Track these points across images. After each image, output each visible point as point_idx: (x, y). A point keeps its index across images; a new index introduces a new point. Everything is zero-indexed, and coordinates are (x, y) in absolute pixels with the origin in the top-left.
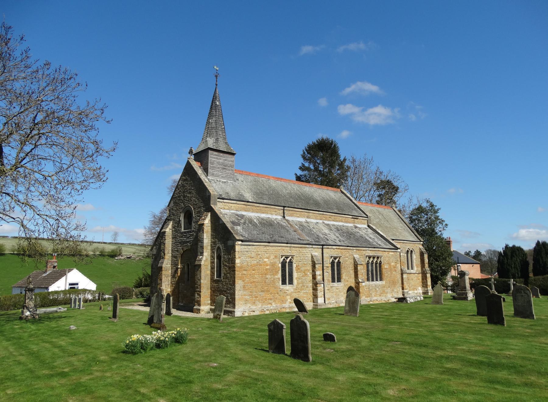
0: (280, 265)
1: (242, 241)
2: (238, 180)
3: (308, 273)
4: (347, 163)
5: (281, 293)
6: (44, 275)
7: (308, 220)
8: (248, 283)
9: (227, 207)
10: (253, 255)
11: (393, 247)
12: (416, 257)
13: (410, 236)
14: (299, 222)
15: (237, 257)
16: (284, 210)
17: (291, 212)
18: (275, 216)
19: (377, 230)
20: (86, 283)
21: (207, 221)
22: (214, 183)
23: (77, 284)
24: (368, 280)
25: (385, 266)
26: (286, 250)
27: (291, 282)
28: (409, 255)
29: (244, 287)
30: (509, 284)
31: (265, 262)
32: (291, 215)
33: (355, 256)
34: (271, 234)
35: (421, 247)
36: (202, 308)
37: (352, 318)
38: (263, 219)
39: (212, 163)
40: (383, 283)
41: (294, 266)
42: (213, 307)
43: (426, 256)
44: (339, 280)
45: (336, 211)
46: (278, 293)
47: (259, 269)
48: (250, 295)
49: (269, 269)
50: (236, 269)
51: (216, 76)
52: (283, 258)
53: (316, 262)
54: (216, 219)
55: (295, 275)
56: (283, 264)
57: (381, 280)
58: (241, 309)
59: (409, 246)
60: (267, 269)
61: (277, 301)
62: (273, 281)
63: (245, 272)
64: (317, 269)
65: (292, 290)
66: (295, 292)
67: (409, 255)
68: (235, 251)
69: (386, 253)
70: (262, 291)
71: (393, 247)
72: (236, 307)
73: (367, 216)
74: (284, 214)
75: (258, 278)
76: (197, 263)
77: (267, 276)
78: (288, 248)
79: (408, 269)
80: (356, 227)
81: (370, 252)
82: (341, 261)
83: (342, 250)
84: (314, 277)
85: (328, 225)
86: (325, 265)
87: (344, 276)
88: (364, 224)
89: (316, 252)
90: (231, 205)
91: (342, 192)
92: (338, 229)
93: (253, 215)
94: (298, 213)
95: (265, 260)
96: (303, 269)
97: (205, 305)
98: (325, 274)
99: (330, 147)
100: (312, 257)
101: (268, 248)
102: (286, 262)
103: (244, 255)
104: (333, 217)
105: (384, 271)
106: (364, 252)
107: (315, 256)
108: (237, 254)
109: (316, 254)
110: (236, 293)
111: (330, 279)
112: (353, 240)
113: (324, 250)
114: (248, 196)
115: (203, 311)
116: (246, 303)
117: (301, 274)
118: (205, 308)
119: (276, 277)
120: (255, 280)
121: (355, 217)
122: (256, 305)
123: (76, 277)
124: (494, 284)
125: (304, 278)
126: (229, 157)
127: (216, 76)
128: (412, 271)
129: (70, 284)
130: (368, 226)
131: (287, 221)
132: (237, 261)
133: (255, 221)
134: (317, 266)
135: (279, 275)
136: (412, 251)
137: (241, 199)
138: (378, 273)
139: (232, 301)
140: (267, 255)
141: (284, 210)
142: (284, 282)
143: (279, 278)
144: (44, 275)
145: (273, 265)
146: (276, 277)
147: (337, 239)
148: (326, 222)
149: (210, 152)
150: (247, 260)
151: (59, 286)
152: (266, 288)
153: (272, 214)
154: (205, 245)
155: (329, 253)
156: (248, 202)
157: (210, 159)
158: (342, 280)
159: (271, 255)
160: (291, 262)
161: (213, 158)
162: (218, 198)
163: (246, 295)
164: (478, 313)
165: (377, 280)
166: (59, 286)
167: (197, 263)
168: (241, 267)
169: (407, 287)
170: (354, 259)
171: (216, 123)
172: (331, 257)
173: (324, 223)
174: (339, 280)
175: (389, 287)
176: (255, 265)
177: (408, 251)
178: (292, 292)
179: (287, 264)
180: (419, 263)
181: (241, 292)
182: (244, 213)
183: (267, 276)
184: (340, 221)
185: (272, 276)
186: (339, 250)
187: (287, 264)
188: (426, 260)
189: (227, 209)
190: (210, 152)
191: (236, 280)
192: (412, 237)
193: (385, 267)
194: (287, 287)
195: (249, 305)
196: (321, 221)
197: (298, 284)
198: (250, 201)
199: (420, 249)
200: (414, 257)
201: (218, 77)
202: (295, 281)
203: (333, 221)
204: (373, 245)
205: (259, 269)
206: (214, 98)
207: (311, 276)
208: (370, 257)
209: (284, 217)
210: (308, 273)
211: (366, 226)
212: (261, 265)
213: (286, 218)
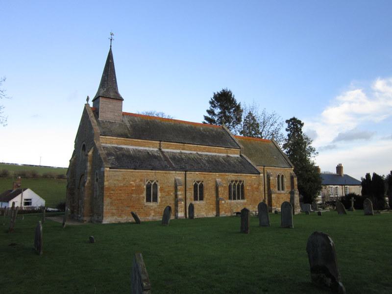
0: (145, 187)
3: (172, 193)
8: (115, 200)
9: (109, 142)
10: (120, 178)
12: (287, 181)
15: (105, 180)
16: (160, 143)
23: (31, 200)
24: (230, 198)
25: (247, 188)
27: (155, 200)
30: (351, 202)
31: (131, 184)
32: (168, 148)
33: (217, 180)
35: (292, 172)
40: (245, 201)
43: (295, 179)
48: (116, 210)
51: (111, 40)
53: (178, 184)
55: (159, 194)
56: (149, 187)
58: (106, 220)
63: (112, 192)
69: (249, 177)
70: (128, 207)
71: (257, 172)
79: (279, 189)
81: (232, 176)
82: (203, 183)
84: (176, 196)
87: (206, 195)
88: (237, 154)
90: (112, 140)
95: (131, 183)
96: (166, 190)
100: (175, 181)
101: (134, 173)
105: (245, 192)
107: (178, 180)
111: (228, 197)
113: (187, 175)
116: (113, 216)
120: (121, 198)
122: (122, 217)
124: (354, 201)
125: (167, 197)
127: (111, 40)
129: (25, 200)
131: (162, 152)
134: (179, 187)
135: (144, 194)
138: (240, 193)
139: (101, 214)
140: (134, 179)
141: (160, 143)
142: (148, 200)
143: (144, 197)
145: (139, 186)
151: (18, 201)
158: (205, 199)
162: (101, 135)
163: (113, 209)
165: (239, 199)
168: (109, 189)
169: (275, 204)
170: (216, 182)
174: (201, 199)
175: (251, 204)
177: (279, 176)
178: (155, 208)
181: (108, 207)
185: (138, 195)
186: (202, 175)
188: (296, 182)
189: (109, 143)
190: (100, 98)
193: (247, 188)
194: (151, 204)
195: (115, 217)
199: (291, 174)
201: (112, 41)
202: (159, 200)
203: (207, 152)
206: (110, 57)
207: (174, 195)
212: (127, 186)
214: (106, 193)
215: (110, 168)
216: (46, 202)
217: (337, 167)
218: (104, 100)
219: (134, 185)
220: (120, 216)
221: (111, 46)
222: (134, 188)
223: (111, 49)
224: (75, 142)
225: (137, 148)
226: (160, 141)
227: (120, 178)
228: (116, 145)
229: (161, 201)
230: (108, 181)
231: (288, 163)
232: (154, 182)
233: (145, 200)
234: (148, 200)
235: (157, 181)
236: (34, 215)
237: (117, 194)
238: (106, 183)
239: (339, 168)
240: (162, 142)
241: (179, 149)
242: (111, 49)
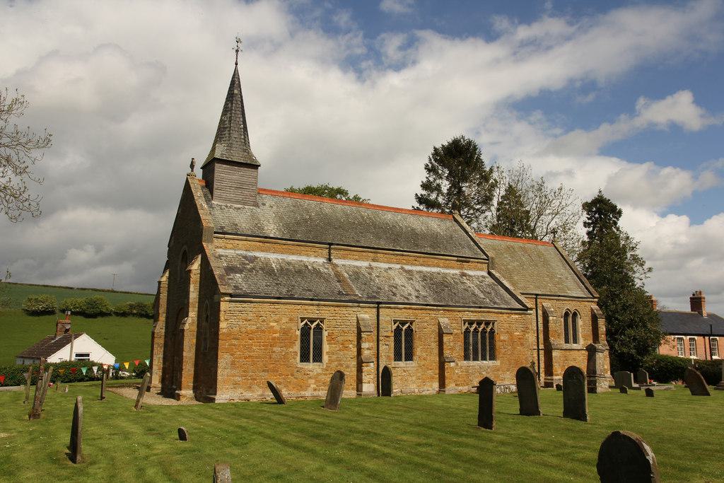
0: (298, 333)
1: (231, 295)
2: (264, 204)
3: (351, 346)
4: (495, 175)
5: (299, 375)
6: (53, 341)
7: (374, 264)
10: (251, 316)
11: (521, 307)
12: (583, 325)
13: (575, 289)
14: (354, 266)
17: (342, 252)
18: (315, 259)
19: (501, 280)
20: (102, 356)
21: (195, 266)
22: (211, 214)
23: (88, 355)
24: (466, 358)
25: (501, 337)
26: (312, 311)
27: (318, 358)
28: (570, 320)
29: (233, 363)
31: (272, 327)
33: (441, 320)
34: (285, 287)
35: (595, 307)
36: (183, 392)
37: (328, 412)
38: (289, 263)
39: (221, 181)
40: (497, 363)
41: (325, 334)
42: (177, 392)
43: (602, 324)
44: (409, 357)
45: (428, 250)
46: (292, 375)
47: (261, 338)
48: (242, 376)
49: (278, 339)
50: (220, 337)
51: (237, 51)
52: (396, 325)
53: (363, 329)
54: (205, 264)
55: (326, 347)
56: (305, 332)
57: (493, 357)
58: (222, 396)
59: (572, 306)
60: (274, 339)
61: (291, 387)
62: (285, 357)
64: (363, 339)
65: (320, 371)
66: (325, 374)
67: (570, 320)
68: (219, 310)
69: (505, 316)
71: (521, 307)
72: (218, 393)
73: (487, 256)
74: (330, 255)
75: (257, 350)
76: (181, 328)
77: (275, 349)
78: (315, 307)
80: (463, 275)
82: (413, 327)
83: (417, 311)
85: (409, 272)
86: (382, 333)
87: (418, 351)
88: (482, 270)
89: (367, 315)
91: (456, 220)
92: (424, 277)
93: (274, 258)
94: (355, 253)
97: (188, 388)
98: (382, 348)
99: (468, 149)
102: (310, 328)
103: (231, 317)
104: (421, 260)
105: (498, 344)
106: (460, 315)
107: (363, 320)
108: (222, 314)
109: (366, 316)
110: (219, 372)
111: (392, 355)
112: (443, 295)
113: (380, 310)
114: (271, 229)
115: (185, 396)
117: (336, 347)
118: (187, 392)
119: (291, 350)
120: (252, 354)
121: (463, 260)
122: (253, 391)
123: (86, 345)
126: (249, 171)
127: (237, 51)
128: (575, 346)
129: (77, 355)
130: (489, 273)
131: (336, 266)
132: (223, 325)
133: (274, 266)
135: (297, 347)
136: (575, 315)
137: (257, 233)
140: (274, 317)
142: (305, 358)
143: (296, 352)
144: (53, 341)
145: (285, 332)
146: (291, 350)
147: (414, 293)
148: (407, 267)
149: (217, 165)
150: (240, 323)
151: (63, 355)
152: (272, 366)
153: (307, 255)
154: (190, 301)
155: (388, 315)
156: (266, 237)
157: (216, 175)
158: (415, 358)
159: (286, 319)
160: (319, 330)
161: (222, 173)
162: (215, 233)
163: (236, 376)
164: (521, 410)
166: (63, 355)
167: (181, 328)
168: (229, 335)
171: (230, 121)
172: (395, 322)
173: (402, 268)
174: (409, 357)
175: (508, 370)
176: (253, 332)
177: (567, 314)
178: (318, 374)
179: (312, 331)
180: (590, 333)
182: (257, 254)
183: (275, 349)
184: (434, 266)
185: (284, 349)
186: (411, 311)
187: (312, 331)
190: (217, 165)
191: (220, 353)
192: (579, 292)
193: (502, 338)
194: (311, 366)
195: (240, 390)
196: (398, 266)
197: (331, 361)
198: (272, 235)
199: (592, 310)
200: (580, 322)
202: (325, 358)
203: (422, 265)
204: (483, 303)
205: (261, 338)
208: (471, 323)
209: (330, 260)
210: (351, 346)
211: (485, 274)
212: (263, 331)
213: (335, 261)
221: (236, 64)
222: (277, 335)
228: (244, 253)
234: (305, 358)
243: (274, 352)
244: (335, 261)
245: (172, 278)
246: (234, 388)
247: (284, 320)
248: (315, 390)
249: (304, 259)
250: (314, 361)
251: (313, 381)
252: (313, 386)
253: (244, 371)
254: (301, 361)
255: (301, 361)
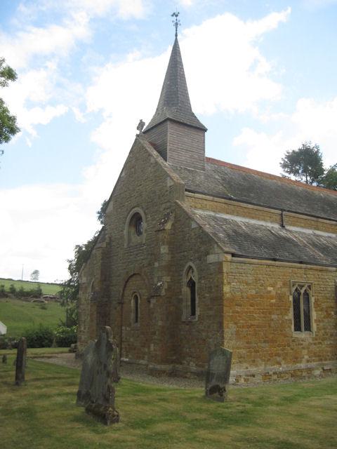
0: (291, 299)
9: (200, 206)
10: (250, 279)
27: (308, 328)
29: (237, 333)
41: (313, 300)
51: (177, 24)
60: (272, 305)
63: (238, 309)
66: (315, 344)
70: (265, 342)
77: (273, 317)
90: (205, 202)
119: (286, 318)
120: (253, 322)
122: (256, 366)
126: (193, 133)
127: (177, 24)
135: (291, 315)
140: (271, 281)
142: (298, 328)
143: (290, 320)
145: (280, 297)
162: (186, 190)
163: (241, 348)
181: (233, 342)
183: (273, 317)
185: (280, 316)
194: (303, 335)
195: (245, 365)
201: (179, 27)
202: (314, 326)
209: (283, 226)
212: (262, 297)
214: (227, 311)
215: (233, 255)
216: (7, 330)
217: (13, 119)
218: (175, 126)
219: (273, 293)
220: (254, 361)
221: (176, 35)
222: (273, 301)
223: (176, 38)
224: (104, 212)
225: (253, 222)
226: (282, 210)
227: (250, 279)
228: (212, 214)
229: (318, 328)
230: (229, 283)
231: (43, 357)
232: (304, 289)
233: (293, 327)
234: (298, 328)
235: (309, 287)
236: (62, 353)
237: (247, 312)
238: (226, 289)
239: (98, 213)
240: (284, 213)
241: (310, 227)
242: (176, 38)
243: (273, 320)
244: (288, 227)
245: (103, 232)
246: (240, 362)
247: (279, 284)
248: (308, 361)
249: (238, 219)
250: (306, 329)
251: (306, 351)
252: (306, 357)
253: (247, 343)
254: (295, 330)
255: (295, 330)
